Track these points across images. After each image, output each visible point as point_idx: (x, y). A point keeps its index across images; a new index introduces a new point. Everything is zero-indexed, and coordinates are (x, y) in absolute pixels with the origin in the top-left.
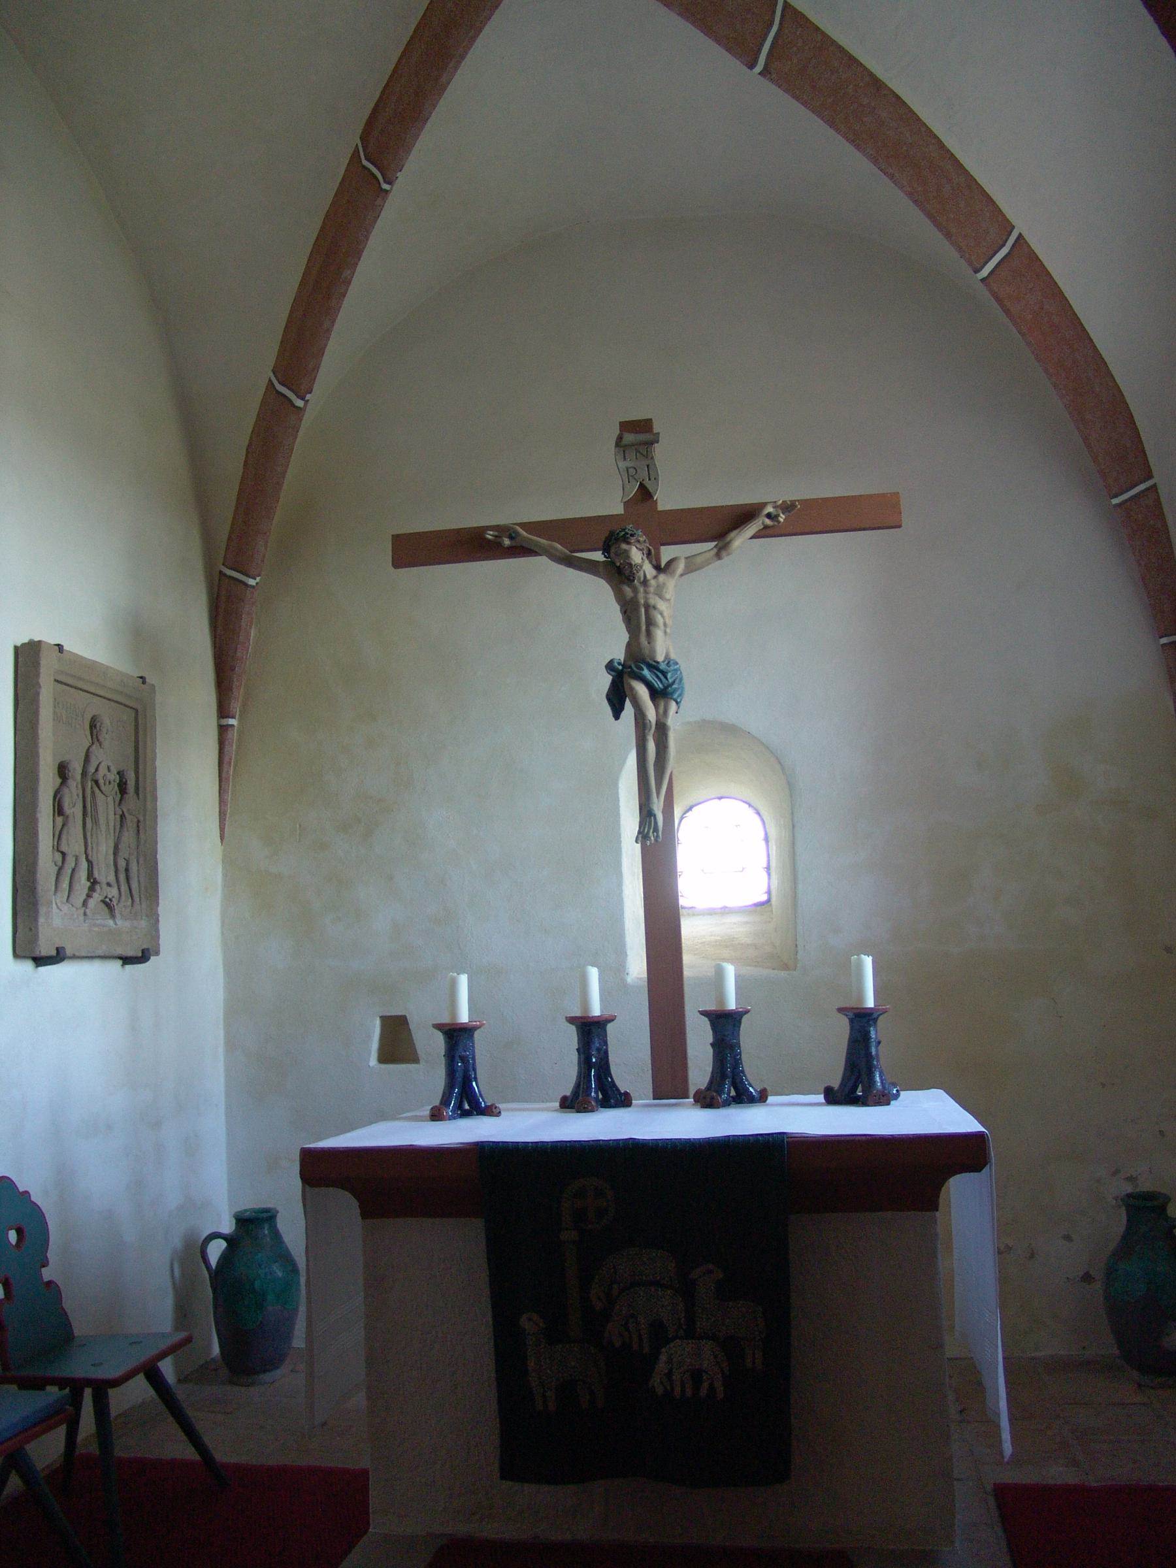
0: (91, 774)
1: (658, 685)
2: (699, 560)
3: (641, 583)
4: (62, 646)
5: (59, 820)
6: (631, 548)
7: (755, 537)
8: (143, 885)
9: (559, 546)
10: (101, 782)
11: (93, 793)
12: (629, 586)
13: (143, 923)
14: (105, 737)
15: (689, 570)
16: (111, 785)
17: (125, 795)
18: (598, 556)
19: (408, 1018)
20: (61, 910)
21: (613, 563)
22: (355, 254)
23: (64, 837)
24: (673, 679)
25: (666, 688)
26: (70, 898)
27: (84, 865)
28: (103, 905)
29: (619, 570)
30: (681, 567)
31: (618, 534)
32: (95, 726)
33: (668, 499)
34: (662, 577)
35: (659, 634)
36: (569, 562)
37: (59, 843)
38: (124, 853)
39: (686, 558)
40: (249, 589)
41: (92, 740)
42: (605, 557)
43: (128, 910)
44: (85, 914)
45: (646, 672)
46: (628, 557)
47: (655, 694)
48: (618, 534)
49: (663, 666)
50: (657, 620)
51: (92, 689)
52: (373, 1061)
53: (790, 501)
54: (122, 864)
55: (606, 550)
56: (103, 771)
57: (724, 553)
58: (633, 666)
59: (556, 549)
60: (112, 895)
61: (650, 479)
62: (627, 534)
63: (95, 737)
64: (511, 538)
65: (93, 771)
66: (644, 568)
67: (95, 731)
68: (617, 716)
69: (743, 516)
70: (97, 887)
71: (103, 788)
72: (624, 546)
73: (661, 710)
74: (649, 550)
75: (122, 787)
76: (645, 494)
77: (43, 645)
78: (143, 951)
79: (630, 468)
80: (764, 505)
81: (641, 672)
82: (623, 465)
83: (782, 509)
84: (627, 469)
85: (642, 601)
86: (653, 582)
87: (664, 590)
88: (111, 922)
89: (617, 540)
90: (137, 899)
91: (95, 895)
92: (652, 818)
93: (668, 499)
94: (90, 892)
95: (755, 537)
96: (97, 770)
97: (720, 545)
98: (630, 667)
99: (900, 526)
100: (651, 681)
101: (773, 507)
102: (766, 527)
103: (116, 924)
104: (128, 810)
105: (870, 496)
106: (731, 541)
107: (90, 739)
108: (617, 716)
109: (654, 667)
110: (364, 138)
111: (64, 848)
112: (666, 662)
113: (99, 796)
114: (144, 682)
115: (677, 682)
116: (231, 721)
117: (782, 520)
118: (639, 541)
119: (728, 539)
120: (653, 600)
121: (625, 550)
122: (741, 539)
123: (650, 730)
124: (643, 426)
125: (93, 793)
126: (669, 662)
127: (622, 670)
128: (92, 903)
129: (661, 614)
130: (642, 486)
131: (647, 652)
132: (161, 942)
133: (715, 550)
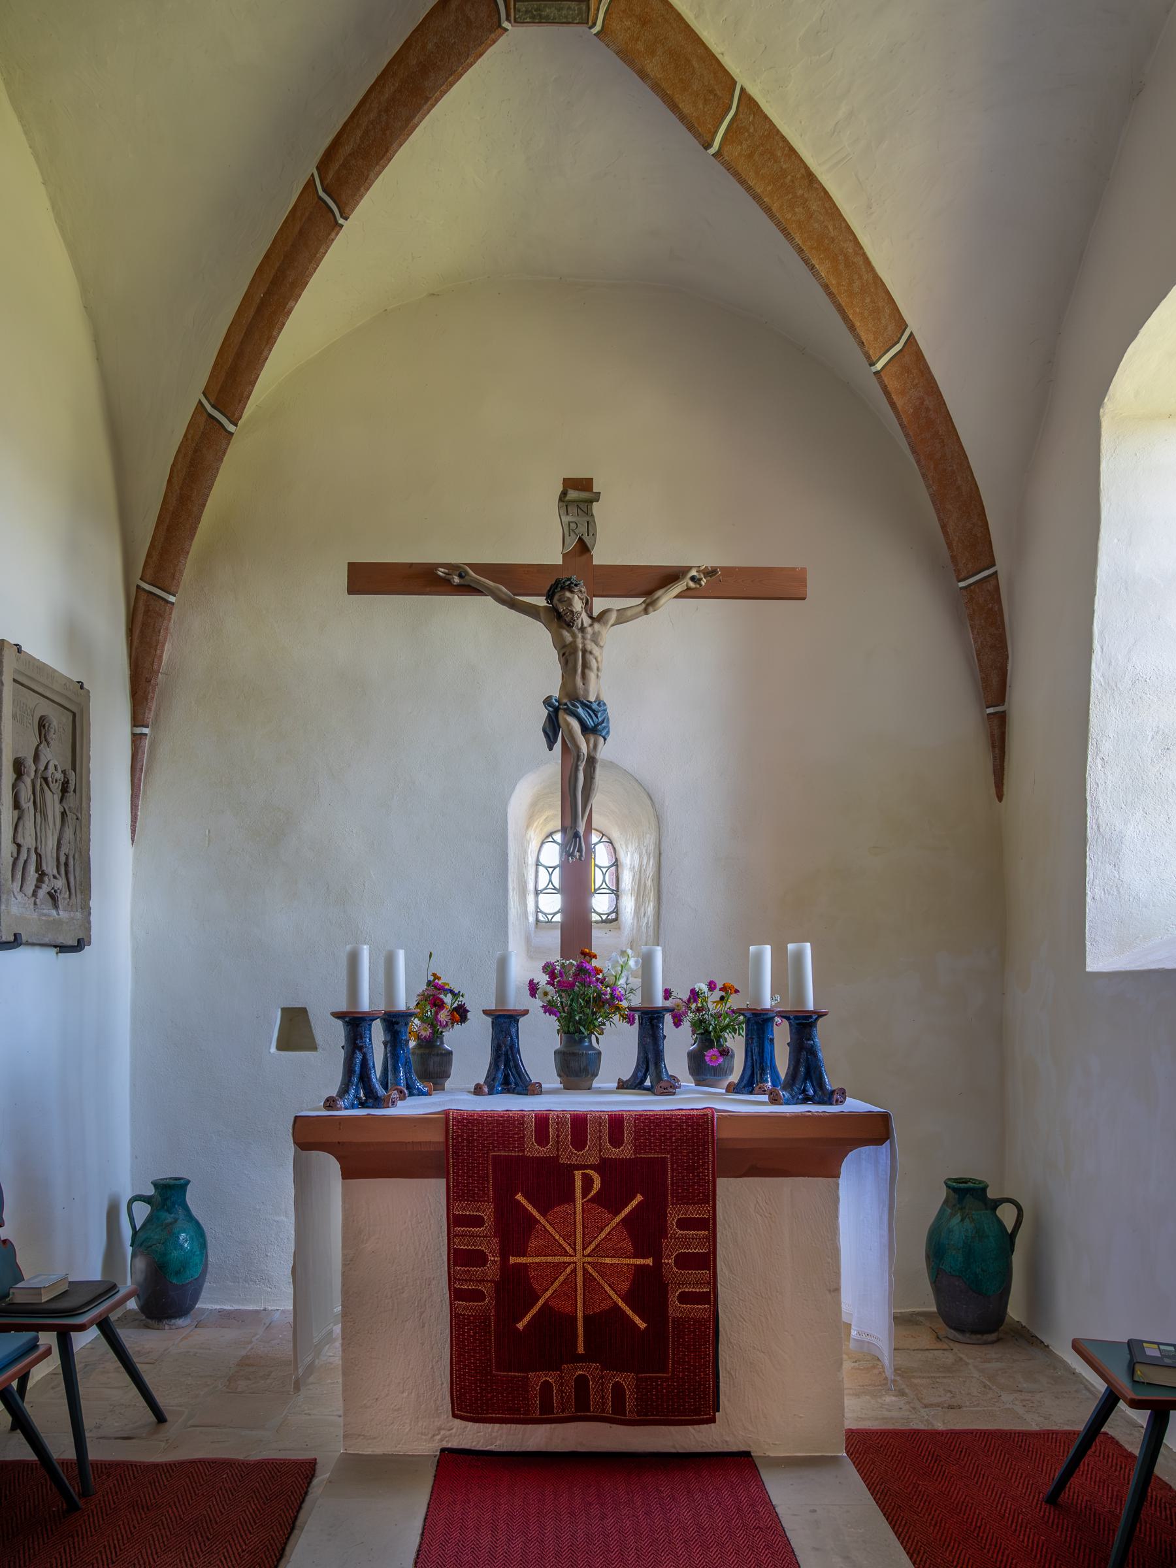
0: (40, 771)
1: (590, 723)
2: (629, 613)
3: (579, 629)
4: (20, 647)
5: (16, 812)
6: (574, 597)
7: (676, 597)
8: (78, 878)
9: (504, 589)
10: (50, 779)
11: (42, 789)
12: (568, 631)
13: (78, 915)
14: (52, 736)
15: (618, 622)
16: (57, 784)
17: (66, 794)
18: (541, 601)
19: (308, 1009)
20: (16, 899)
21: (555, 610)
22: (300, 283)
23: (20, 829)
24: (602, 718)
25: (596, 726)
26: (23, 889)
27: (34, 857)
28: (48, 896)
29: (559, 616)
30: (613, 617)
31: (564, 583)
32: (44, 726)
33: (602, 556)
34: (597, 626)
35: (592, 676)
36: (513, 605)
37: (16, 835)
38: (64, 850)
39: (618, 610)
40: (169, 605)
41: (40, 740)
42: (548, 602)
43: (66, 902)
44: (35, 904)
45: (580, 710)
46: (571, 605)
47: (585, 729)
48: (564, 583)
49: (595, 706)
50: (592, 665)
51: (41, 690)
52: (273, 1050)
53: (711, 567)
54: (63, 859)
55: (550, 596)
56: (51, 769)
57: (651, 609)
58: (568, 704)
59: (501, 590)
60: (58, 887)
61: (588, 535)
62: (573, 583)
63: (43, 736)
64: (460, 576)
65: (43, 769)
66: (582, 615)
67: (43, 733)
68: (551, 748)
69: (669, 577)
70: (46, 879)
71: (51, 785)
72: (568, 594)
73: (591, 746)
74: (587, 600)
75: (64, 789)
76: (583, 548)
77: (5, 644)
78: (79, 941)
79: (572, 522)
80: (690, 568)
81: (576, 709)
82: (566, 519)
83: (704, 574)
84: (569, 523)
85: (580, 646)
86: (589, 630)
87: (600, 638)
88: (54, 912)
89: (563, 588)
90: (73, 891)
91: (44, 886)
92: (578, 839)
93: (602, 556)
94: (39, 883)
95: (676, 597)
96: (46, 768)
97: (648, 601)
98: (566, 704)
99: (804, 599)
100: (584, 719)
101: (697, 572)
102: (689, 589)
103: (59, 915)
104: (70, 808)
105: (782, 569)
106: (658, 598)
107: (39, 740)
108: (551, 748)
109: (587, 706)
110: (322, 166)
111: (20, 840)
112: (597, 703)
113: (48, 793)
114: (82, 687)
115: (606, 720)
116: (146, 730)
117: (703, 584)
118: (581, 591)
119: (656, 596)
120: (590, 646)
121: (569, 598)
122: (668, 599)
123: (582, 762)
124: (585, 484)
125: (42, 789)
126: (599, 703)
127: (558, 706)
128: (42, 893)
129: (596, 659)
130: (581, 540)
131: (581, 692)
132: (91, 933)
133: (644, 605)
